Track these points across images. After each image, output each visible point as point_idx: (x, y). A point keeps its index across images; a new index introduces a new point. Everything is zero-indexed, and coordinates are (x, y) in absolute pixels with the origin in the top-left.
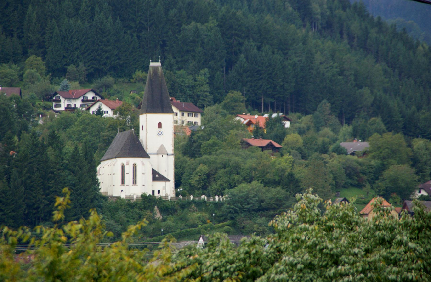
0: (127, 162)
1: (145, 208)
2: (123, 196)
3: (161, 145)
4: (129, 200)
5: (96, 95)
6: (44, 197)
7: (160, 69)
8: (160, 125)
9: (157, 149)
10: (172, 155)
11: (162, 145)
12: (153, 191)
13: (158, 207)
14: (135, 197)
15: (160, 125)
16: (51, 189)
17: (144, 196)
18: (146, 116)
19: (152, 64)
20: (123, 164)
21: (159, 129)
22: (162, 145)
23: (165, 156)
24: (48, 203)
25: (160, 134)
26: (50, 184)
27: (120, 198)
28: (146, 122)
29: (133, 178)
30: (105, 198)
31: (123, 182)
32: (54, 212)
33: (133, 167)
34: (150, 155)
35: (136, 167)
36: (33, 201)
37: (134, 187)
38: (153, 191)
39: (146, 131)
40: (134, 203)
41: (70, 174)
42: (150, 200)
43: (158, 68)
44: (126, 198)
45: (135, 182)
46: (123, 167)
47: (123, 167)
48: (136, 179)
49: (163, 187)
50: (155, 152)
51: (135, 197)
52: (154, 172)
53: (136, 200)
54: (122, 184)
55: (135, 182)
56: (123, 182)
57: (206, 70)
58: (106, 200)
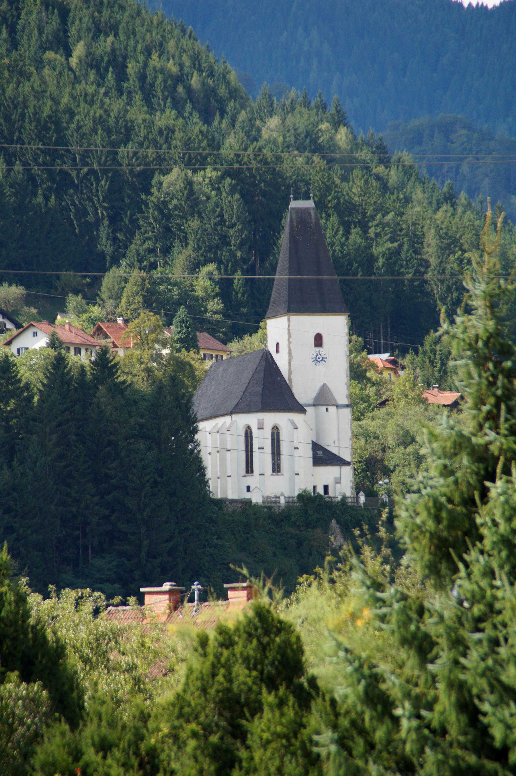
0: (259, 423)
1: (308, 525)
2: (256, 498)
3: (322, 384)
4: (270, 508)
5: (3, 318)
6: (96, 499)
7: (313, 214)
8: (319, 340)
9: (313, 395)
10: (347, 406)
11: (325, 385)
12: (315, 487)
13: (338, 523)
14: (282, 501)
15: (319, 340)
16: (113, 482)
17: (303, 497)
18: (289, 320)
19: (293, 204)
20: (249, 427)
21: (317, 349)
22: (325, 385)
23: (332, 409)
24: (106, 512)
25: (319, 360)
26: (109, 469)
27: (251, 502)
28: (289, 333)
29: (273, 459)
30: (220, 503)
31: (249, 469)
32: (9, 557)
33: (273, 434)
34: (306, 408)
35: (278, 433)
36: (74, 509)
37: (276, 478)
38: (315, 487)
39: (290, 354)
40: (281, 514)
41: (149, 449)
42: (319, 505)
43: (309, 214)
44: (263, 502)
45: (276, 468)
46: (248, 435)
47: (248, 435)
48: (279, 460)
49: (336, 478)
50: (311, 402)
51: (282, 501)
52: (316, 447)
53: (286, 507)
54: (247, 472)
55: (276, 468)
56: (249, 469)
57: (211, 267)
58: (220, 509)
